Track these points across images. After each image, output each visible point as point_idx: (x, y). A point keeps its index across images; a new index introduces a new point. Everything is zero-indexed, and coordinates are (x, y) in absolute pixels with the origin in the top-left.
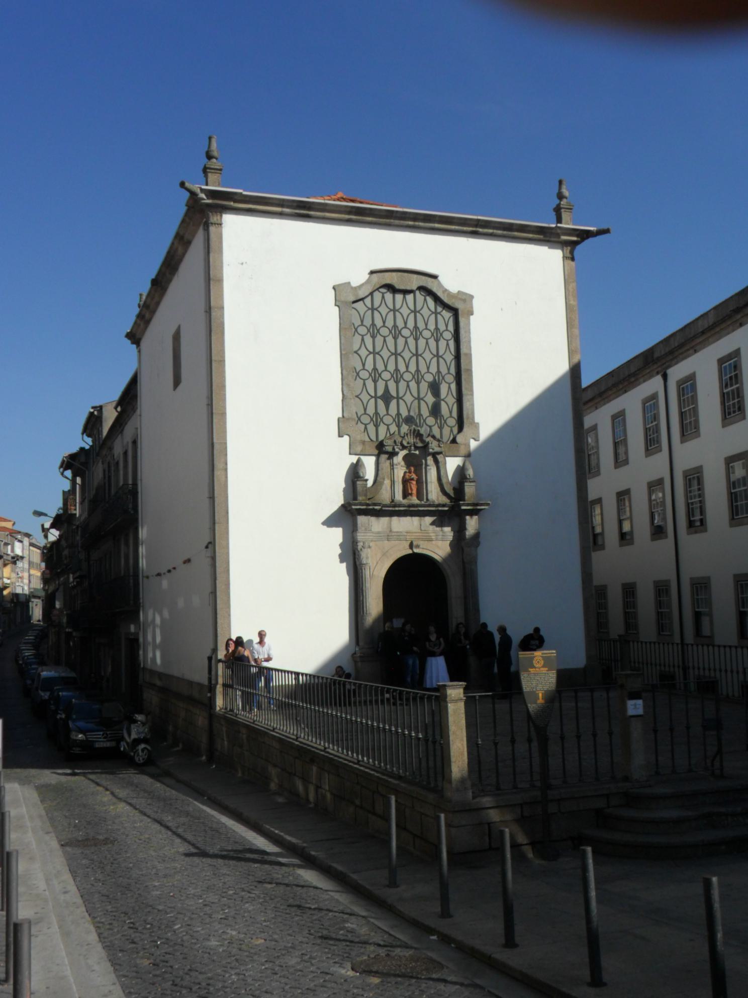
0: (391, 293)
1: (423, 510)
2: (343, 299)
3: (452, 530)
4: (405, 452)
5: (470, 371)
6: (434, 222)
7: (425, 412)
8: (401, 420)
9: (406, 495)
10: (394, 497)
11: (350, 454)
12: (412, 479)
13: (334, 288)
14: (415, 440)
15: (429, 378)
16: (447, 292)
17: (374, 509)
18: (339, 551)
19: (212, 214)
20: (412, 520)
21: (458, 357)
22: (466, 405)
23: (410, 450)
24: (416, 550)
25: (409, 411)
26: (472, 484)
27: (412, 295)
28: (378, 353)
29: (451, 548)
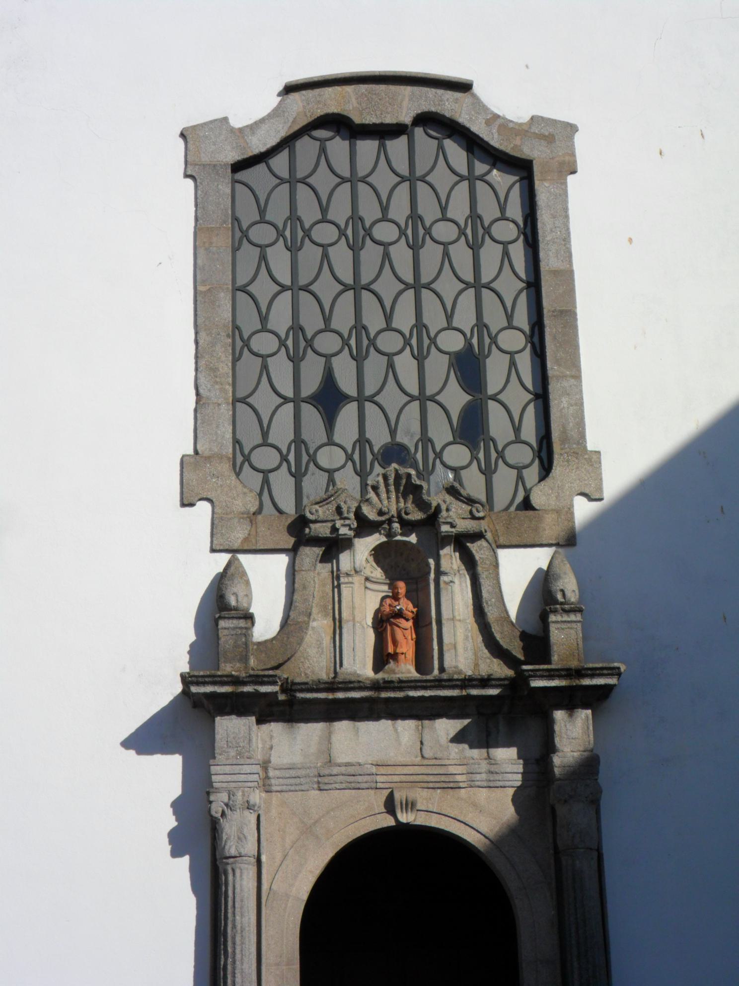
0: (343, 139)
1: (422, 698)
2: (205, 159)
3: (520, 757)
4: (376, 539)
5: (568, 315)
7: (440, 433)
8: (369, 457)
9: (382, 658)
10: (341, 665)
11: (213, 550)
12: (399, 614)
13: (183, 135)
14: (402, 505)
15: (453, 342)
16: (499, 122)
17: (257, 694)
18: (174, 817)
21: (534, 285)
22: (559, 404)
23: (390, 534)
24: (404, 817)
25: (393, 432)
26: (572, 617)
27: (403, 139)
28: (306, 289)
29: (517, 811)
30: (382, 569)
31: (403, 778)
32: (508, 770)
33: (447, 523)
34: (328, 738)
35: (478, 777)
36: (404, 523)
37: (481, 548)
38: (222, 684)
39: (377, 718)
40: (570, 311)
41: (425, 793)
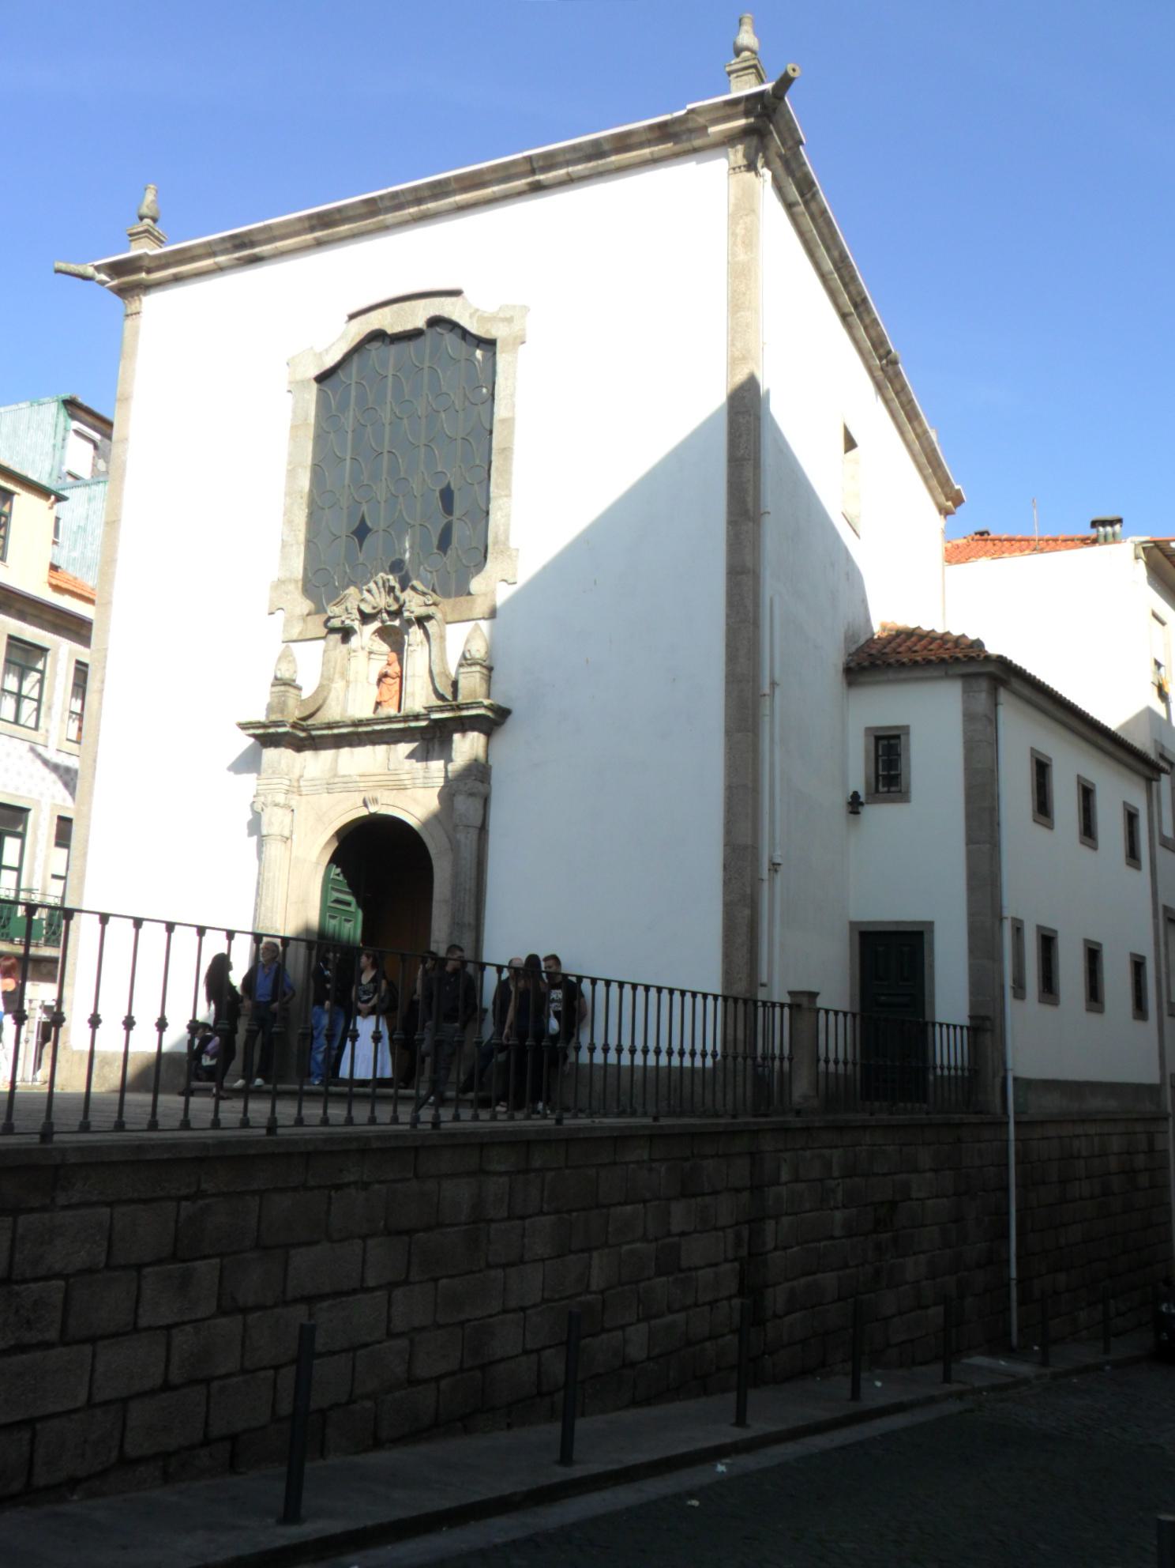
6: (454, 193)
16: (479, 313)
19: (129, 301)
20: (374, 753)
23: (383, 622)
29: (440, 803)
30: (388, 644)
31: (374, 784)
32: (435, 776)
33: (408, 610)
34: (336, 761)
35: (418, 781)
36: (389, 613)
37: (433, 625)
38: (258, 728)
39: (364, 745)
40: (509, 448)
41: (386, 793)
